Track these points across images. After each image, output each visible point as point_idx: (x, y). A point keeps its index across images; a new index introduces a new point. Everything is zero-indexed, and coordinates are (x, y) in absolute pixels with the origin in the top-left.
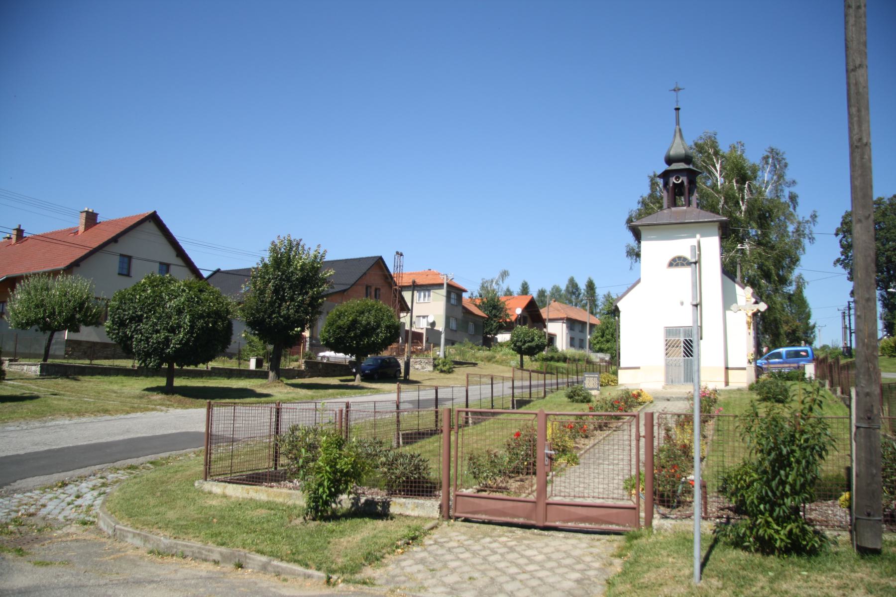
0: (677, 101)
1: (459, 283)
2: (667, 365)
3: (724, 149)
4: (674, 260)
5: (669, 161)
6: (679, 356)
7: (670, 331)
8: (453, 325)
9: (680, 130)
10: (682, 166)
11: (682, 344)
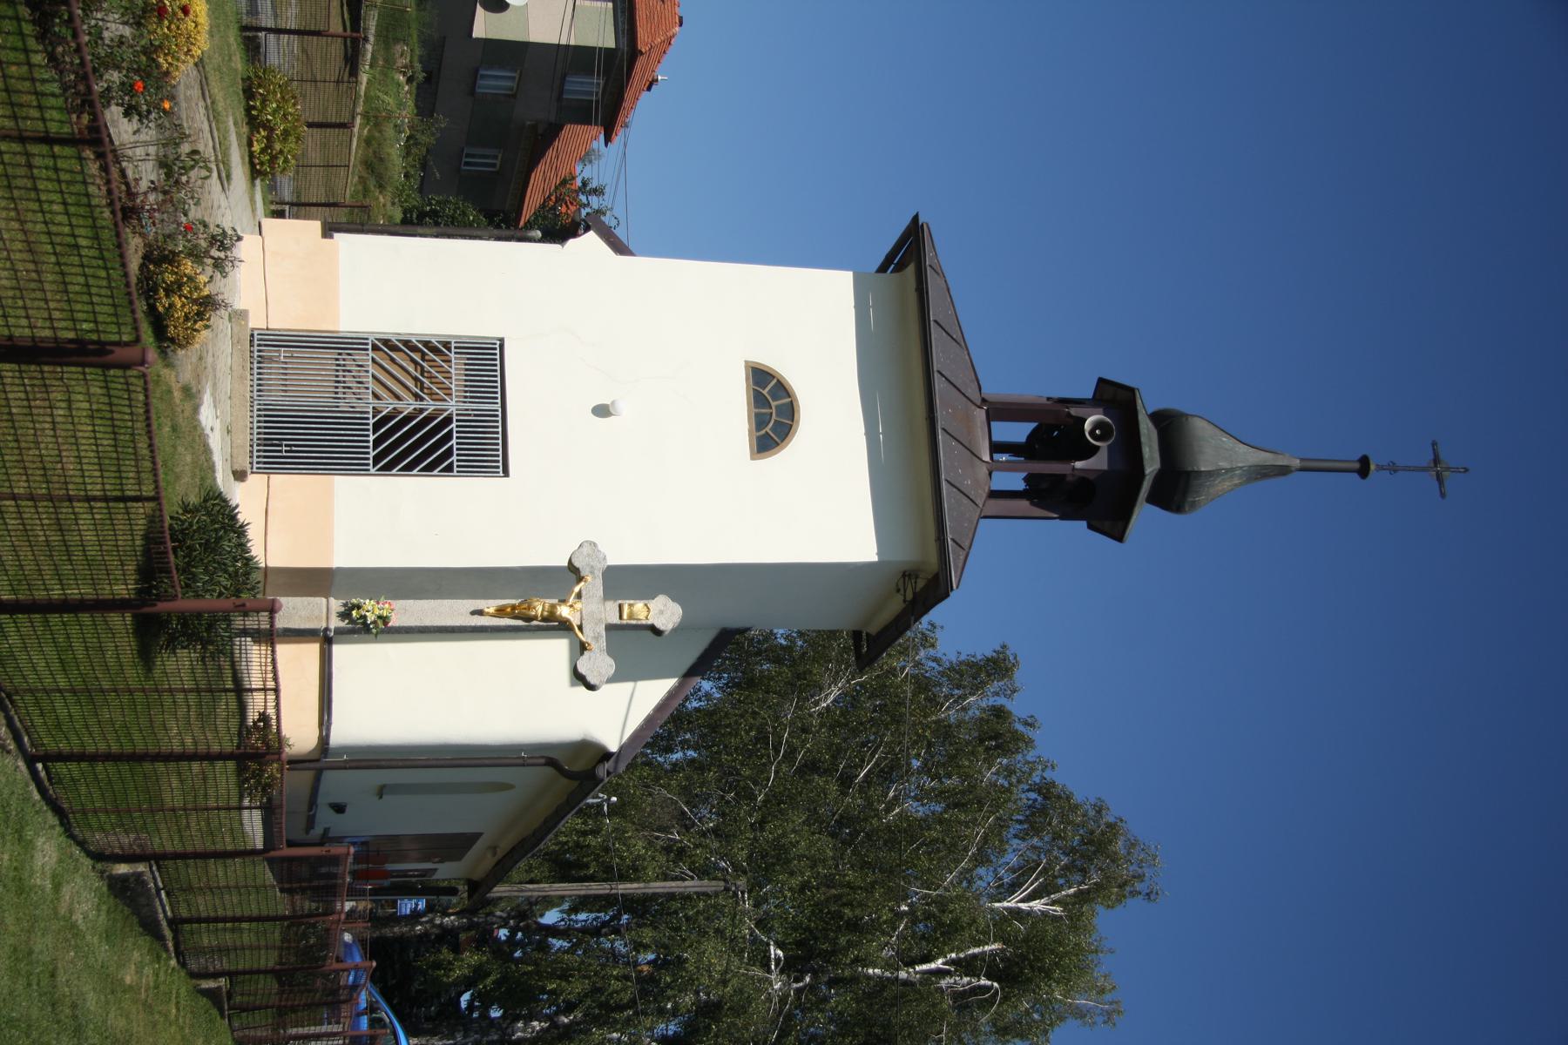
0: (1393, 468)
1: (643, 111)
2: (344, 345)
3: (1105, 921)
4: (782, 389)
5: (1168, 423)
6: (370, 398)
7: (486, 359)
8: (495, 82)
9: (1284, 471)
10: (1152, 463)
11: (430, 406)
